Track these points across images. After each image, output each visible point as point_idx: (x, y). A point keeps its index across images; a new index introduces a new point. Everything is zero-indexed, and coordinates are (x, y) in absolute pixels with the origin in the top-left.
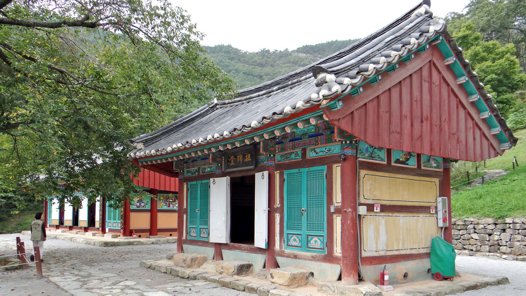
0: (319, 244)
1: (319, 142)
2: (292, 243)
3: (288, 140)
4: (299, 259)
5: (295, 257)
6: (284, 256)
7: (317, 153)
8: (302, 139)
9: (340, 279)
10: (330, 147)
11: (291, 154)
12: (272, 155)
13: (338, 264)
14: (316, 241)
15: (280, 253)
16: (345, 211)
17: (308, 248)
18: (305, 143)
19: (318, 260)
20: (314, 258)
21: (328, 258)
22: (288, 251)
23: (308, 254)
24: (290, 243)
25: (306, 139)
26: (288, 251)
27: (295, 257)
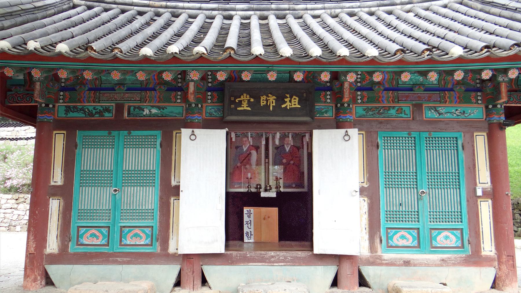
0: (453, 240)
1: (448, 100)
2: (397, 240)
3: (87, 88)
4: (415, 265)
5: (407, 263)
6: (381, 264)
7: (440, 114)
8: (115, 90)
9: (178, 284)
10: (463, 109)
11: (389, 108)
12: (51, 106)
13: (491, 266)
14: (447, 237)
15: (371, 260)
16: (507, 195)
17: (435, 249)
18: (419, 97)
19: (454, 265)
20: (444, 262)
21: (473, 260)
22: (388, 256)
23: (435, 257)
24: (391, 243)
25: (418, 92)
26: (388, 256)
27: (407, 263)
